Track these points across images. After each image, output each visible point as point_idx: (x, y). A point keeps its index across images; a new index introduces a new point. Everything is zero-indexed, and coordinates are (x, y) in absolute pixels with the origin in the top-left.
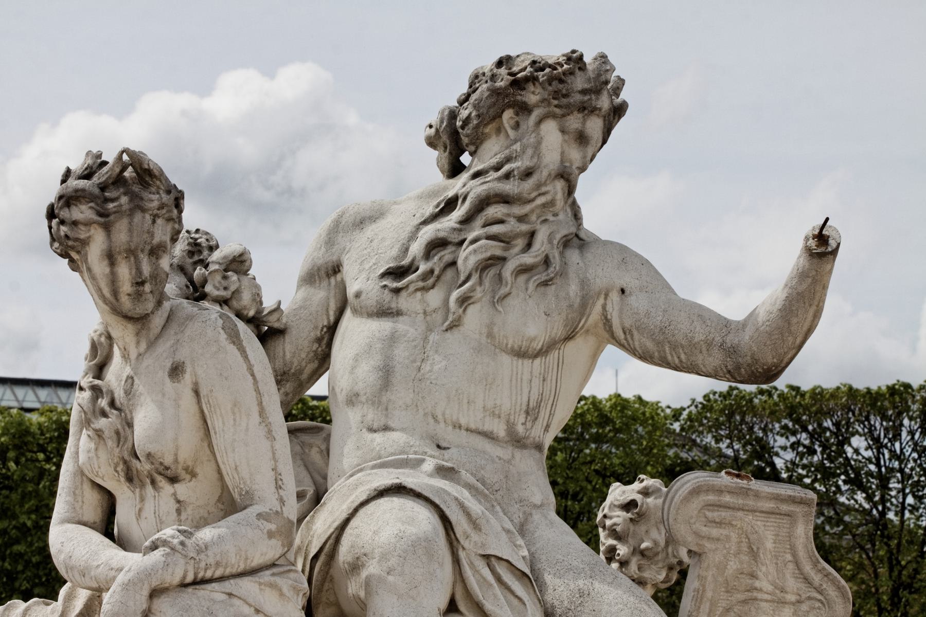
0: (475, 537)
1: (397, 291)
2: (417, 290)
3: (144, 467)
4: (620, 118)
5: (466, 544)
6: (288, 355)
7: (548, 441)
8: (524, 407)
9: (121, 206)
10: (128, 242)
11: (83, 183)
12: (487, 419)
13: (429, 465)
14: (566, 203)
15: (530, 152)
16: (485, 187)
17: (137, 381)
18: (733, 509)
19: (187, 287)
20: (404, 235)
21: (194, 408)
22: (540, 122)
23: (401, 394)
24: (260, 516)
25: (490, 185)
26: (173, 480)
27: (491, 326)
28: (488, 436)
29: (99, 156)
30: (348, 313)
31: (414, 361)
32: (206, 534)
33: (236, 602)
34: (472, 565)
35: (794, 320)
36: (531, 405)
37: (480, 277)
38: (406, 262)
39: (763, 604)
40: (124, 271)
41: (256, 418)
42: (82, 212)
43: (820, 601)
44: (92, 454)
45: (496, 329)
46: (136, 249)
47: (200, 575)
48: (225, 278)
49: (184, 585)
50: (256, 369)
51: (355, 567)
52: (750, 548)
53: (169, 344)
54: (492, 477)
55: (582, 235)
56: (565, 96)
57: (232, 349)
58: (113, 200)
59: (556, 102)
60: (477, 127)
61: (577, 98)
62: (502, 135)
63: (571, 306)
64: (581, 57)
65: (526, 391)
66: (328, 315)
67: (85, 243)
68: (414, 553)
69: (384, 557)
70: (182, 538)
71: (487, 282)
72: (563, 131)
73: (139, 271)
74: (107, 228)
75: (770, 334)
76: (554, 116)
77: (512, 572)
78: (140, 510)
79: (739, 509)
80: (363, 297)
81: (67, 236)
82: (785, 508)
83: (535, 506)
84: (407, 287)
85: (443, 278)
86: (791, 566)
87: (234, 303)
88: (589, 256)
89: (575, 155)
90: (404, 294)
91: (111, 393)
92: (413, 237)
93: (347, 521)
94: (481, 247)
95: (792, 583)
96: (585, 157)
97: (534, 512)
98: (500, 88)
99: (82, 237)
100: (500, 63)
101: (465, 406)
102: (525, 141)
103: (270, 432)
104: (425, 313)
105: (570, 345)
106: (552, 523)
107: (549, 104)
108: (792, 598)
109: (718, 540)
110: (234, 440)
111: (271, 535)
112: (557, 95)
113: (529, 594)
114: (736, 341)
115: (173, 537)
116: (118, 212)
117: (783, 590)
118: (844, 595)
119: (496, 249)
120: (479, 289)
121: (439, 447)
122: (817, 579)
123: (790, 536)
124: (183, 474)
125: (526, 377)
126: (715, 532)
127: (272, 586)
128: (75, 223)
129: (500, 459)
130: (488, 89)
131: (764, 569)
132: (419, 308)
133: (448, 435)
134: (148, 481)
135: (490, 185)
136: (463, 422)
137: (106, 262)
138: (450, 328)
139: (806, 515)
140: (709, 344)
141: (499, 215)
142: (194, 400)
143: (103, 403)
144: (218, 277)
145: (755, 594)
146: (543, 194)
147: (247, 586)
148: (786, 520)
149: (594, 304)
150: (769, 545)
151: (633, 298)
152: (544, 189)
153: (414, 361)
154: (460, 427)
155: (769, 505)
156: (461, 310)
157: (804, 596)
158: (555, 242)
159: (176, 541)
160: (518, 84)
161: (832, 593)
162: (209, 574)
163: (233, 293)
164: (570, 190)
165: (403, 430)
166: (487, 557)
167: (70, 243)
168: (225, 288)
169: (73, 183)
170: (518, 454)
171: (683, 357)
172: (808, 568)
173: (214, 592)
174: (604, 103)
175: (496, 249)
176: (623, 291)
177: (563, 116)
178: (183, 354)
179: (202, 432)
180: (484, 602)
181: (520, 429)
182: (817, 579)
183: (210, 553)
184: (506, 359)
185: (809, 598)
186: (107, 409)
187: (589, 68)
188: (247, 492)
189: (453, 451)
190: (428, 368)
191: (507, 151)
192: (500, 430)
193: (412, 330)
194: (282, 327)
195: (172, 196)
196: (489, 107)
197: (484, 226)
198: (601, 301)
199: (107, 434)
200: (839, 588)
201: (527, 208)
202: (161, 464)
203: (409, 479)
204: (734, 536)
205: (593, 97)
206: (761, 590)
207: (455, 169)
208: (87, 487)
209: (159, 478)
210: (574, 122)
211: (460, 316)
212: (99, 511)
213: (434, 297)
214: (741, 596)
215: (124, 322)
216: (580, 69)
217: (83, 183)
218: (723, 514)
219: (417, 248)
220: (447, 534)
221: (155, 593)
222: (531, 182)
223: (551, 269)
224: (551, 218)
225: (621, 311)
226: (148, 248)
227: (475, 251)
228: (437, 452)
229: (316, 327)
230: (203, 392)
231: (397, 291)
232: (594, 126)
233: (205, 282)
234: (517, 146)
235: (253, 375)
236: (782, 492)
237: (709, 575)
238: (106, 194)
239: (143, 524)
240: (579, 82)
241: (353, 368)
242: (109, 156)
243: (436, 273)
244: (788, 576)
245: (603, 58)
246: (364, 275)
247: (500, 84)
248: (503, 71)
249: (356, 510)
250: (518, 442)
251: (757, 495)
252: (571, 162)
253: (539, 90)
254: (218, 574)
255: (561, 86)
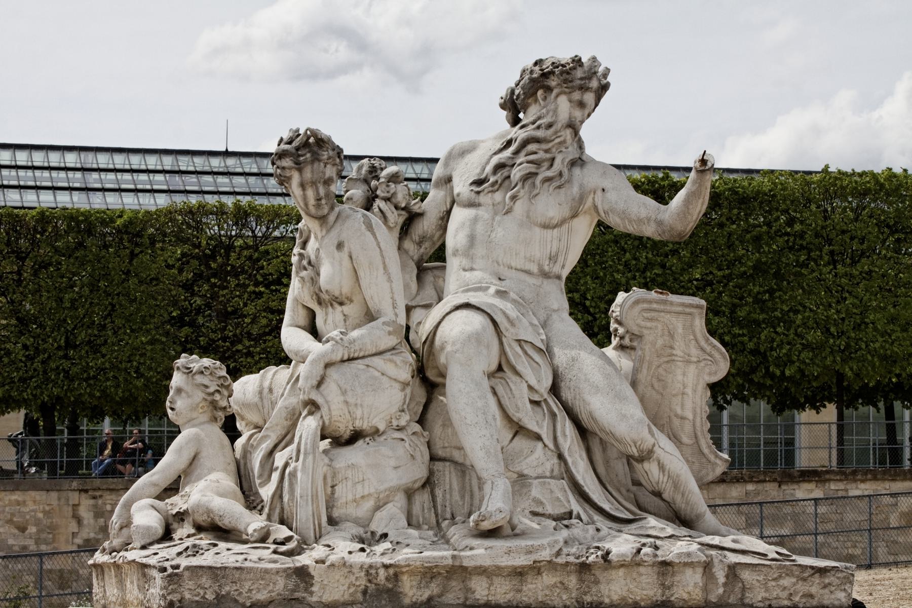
0: (512, 330)
1: (478, 193)
2: (489, 192)
3: (325, 297)
4: (606, 91)
5: (507, 334)
6: (426, 228)
7: (565, 273)
8: (548, 256)
9: (306, 158)
10: (311, 178)
11: (287, 147)
12: (527, 263)
13: (492, 290)
14: (573, 140)
15: (551, 113)
16: (526, 134)
17: (321, 251)
18: (658, 311)
19: (368, 191)
20: (484, 161)
21: (349, 265)
22: (557, 96)
23: (480, 251)
24: (384, 323)
25: (529, 132)
26: (341, 304)
27: (528, 212)
28: (528, 272)
29: (298, 130)
30: (455, 204)
31: (487, 232)
32: (355, 334)
33: (371, 369)
34: (510, 346)
35: (691, 207)
36: (552, 255)
37: (523, 184)
38: (483, 177)
39: (678, 363)
40: (310, 193)
41: (381, 271)
42: (287, 162)
43: (711, 361)
44: (300, 290)
45: (531, 214)
46: (316, 180)
47: (352, 356)
48: (388, 186)
49: (343, 361)
50: (382, 245)
51: (442, 348)
52: (669, 332)
53: (337, 231)
54: (528, 295)
55: (584, 158)
56: (571, 81)
57: (368, 234)
58: (302, 156)
59: (565, 85)
60: (524, 99)
61: (579, 82)
62: (538, 104)
63: (573, 199)
64: (580, 60)
65: (549, 247)
66: (446, 205)
67: (289, 179)
68: (470, 341)
69: (454, 343)
70: (341, 336)
71: (527, 187)
72: (570, 101)
73: (318, 193)
74: (300, 170)
75: (678, 214)
76: (565, 93)
77: (534, 349)
78: (326, 320)
79: (661, 312)
80: (461, 196)
81: (280, 175)
82: (688, 310)
83: (554, 311)
84: (483, 190)
85: (503, 185)
86: (693, 342)
87: (393, 200)
88: (585, 170)
89: (578, 114)
90: (482, 194)
91: (309, 257)
92: (488, 162)
93: (439, 323)
94: (523, 168)
95: (694, 352)
96: (583, 115)
97: (553, 314)
98: (535, 78)
99: (288, 175)
100: (536, 64)
101: (514, 257)
102: (548, 107)
103: (389, 278)
104: (493, 205)
105: (576, 220)
106: (563, 320)
107: (562, 87)
108: (695, 359)
109: (651, 328)
110: (370, 283)
111: (390, 333)
112: (565, 81)
113: (543, 360)
114: (662, 218)
115: (337, 336)
116: (305, 162)
117: (689, 355)
118: (724, 358)
119: (532, 168)
120: (522, 191)
121: (500, 279)
122: (708, 348)
123: (692, 325)
124: (346, 301)
125: (549, 239)
126: (649, 324)
127: (391, 361)
128: (284, 168)
129: (534, 285)
130: (529, 79)
131: (678, 344)
132: (490, 202)
133: (505, 272)
134: (329, 305)
135: (529, 132)
136: (513, 265)
137: (300, 189)
138: (506, 213)
139: (700, 314)
140: (649, 220)
141: (534, 149)
142: (350, 261)
143: (305, 262)
144: (384, 186)
145: (673, 358)
146: (559, 137)
147: (377, 361)
148: (689, 317)
149: (587, 197)
150: (680, 330)
151: (609, 194)
152: (559, 134)
153: (487, 232)
154: (512, 268)
155: (680, 309)
156: (512, 203)
157: (701, 358)
158: (566, 164)
159: (338, 338)
160: (545, 75)
161: (717, 355)
162: (356, 355)
163: (392, 194)
164: (576, 133)
165: (481, 270)
166: (519, 341)
167: (282, 178)
168: (388, 192)
169: (284, 147)
170: (546, 282)
171: (635, 226)
172: (703, 343)
173: (359, 365)
174: (594, 84)
175: (532, 168)
176: (603, 190)
177: (570, 93)
178: (344, 237)
179: (354, 279)
180: (516, 366)
181: (546, 268)
182: (708, 348)
183: (356, 344)
184: (537, 230)
185: (705, 359)
186: (307, 266)
187: (585, 65)
188: (378, 311)
189: (507, 281)
190: (494, 236)
191: (539, 114)
192: (534, 269)
193: (486, 214)
194: (422, 212)
195: (335, 152)
196: (529, 89)
197: (526, 156)
198: (592, 195)
199: (306, 279)
200: (722, 354)
201: (550, 145)
202: (333, 296)
203: (474, 298)
204: (660, 326)
205: (587, 81)
206: (676, 355)
207: (515, 121)
208: (300, 307)
209: (334, 303)
210: (576, 96)
211: (512, 207)
212: (307, 319)
213: (498, 196)
214: (666, 359)
215: (313, 219)
216: (580, 66)
217: (287, 147)
218: (653, 314)
219: (489, 168)
220: (496, 329)
221: (327, 366)
222: (552, 130)
223: (563, 179)
224: (564, 150)
225: (602, 201)
226: (322, 180)
227: (520, 170)
228: (498, 282)
229: (440, 212)
230: (354, 257)
231: (478, 193)
232: (589, 97)
233: (377, 189)
234: (544, 111)
235: (380, 248)
236: (686, 301)
237: (647, 347)
238: (299, 152)
239: (327, 327)
240: (579, 73)
241: (455, 236)
242: (302, 132)
243: (499, 182)
244: (692, 347)
245: (594, 59)
246: (462, 184)
247: (535, 75)
248: (537, 68)
249: (444, 317)
250: (545, 275)
251: (672, 303)
252: (575, 118)
253: (556, 79)
254: (361, 354)
255: (568, 76)
